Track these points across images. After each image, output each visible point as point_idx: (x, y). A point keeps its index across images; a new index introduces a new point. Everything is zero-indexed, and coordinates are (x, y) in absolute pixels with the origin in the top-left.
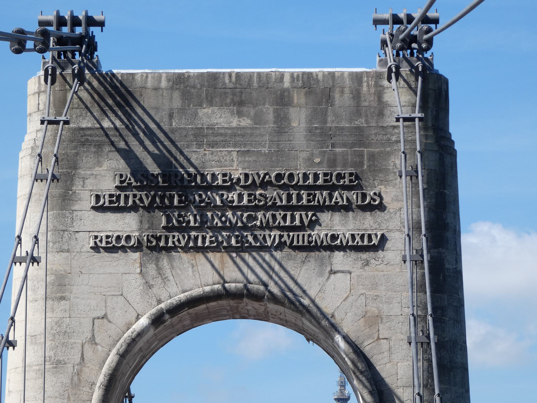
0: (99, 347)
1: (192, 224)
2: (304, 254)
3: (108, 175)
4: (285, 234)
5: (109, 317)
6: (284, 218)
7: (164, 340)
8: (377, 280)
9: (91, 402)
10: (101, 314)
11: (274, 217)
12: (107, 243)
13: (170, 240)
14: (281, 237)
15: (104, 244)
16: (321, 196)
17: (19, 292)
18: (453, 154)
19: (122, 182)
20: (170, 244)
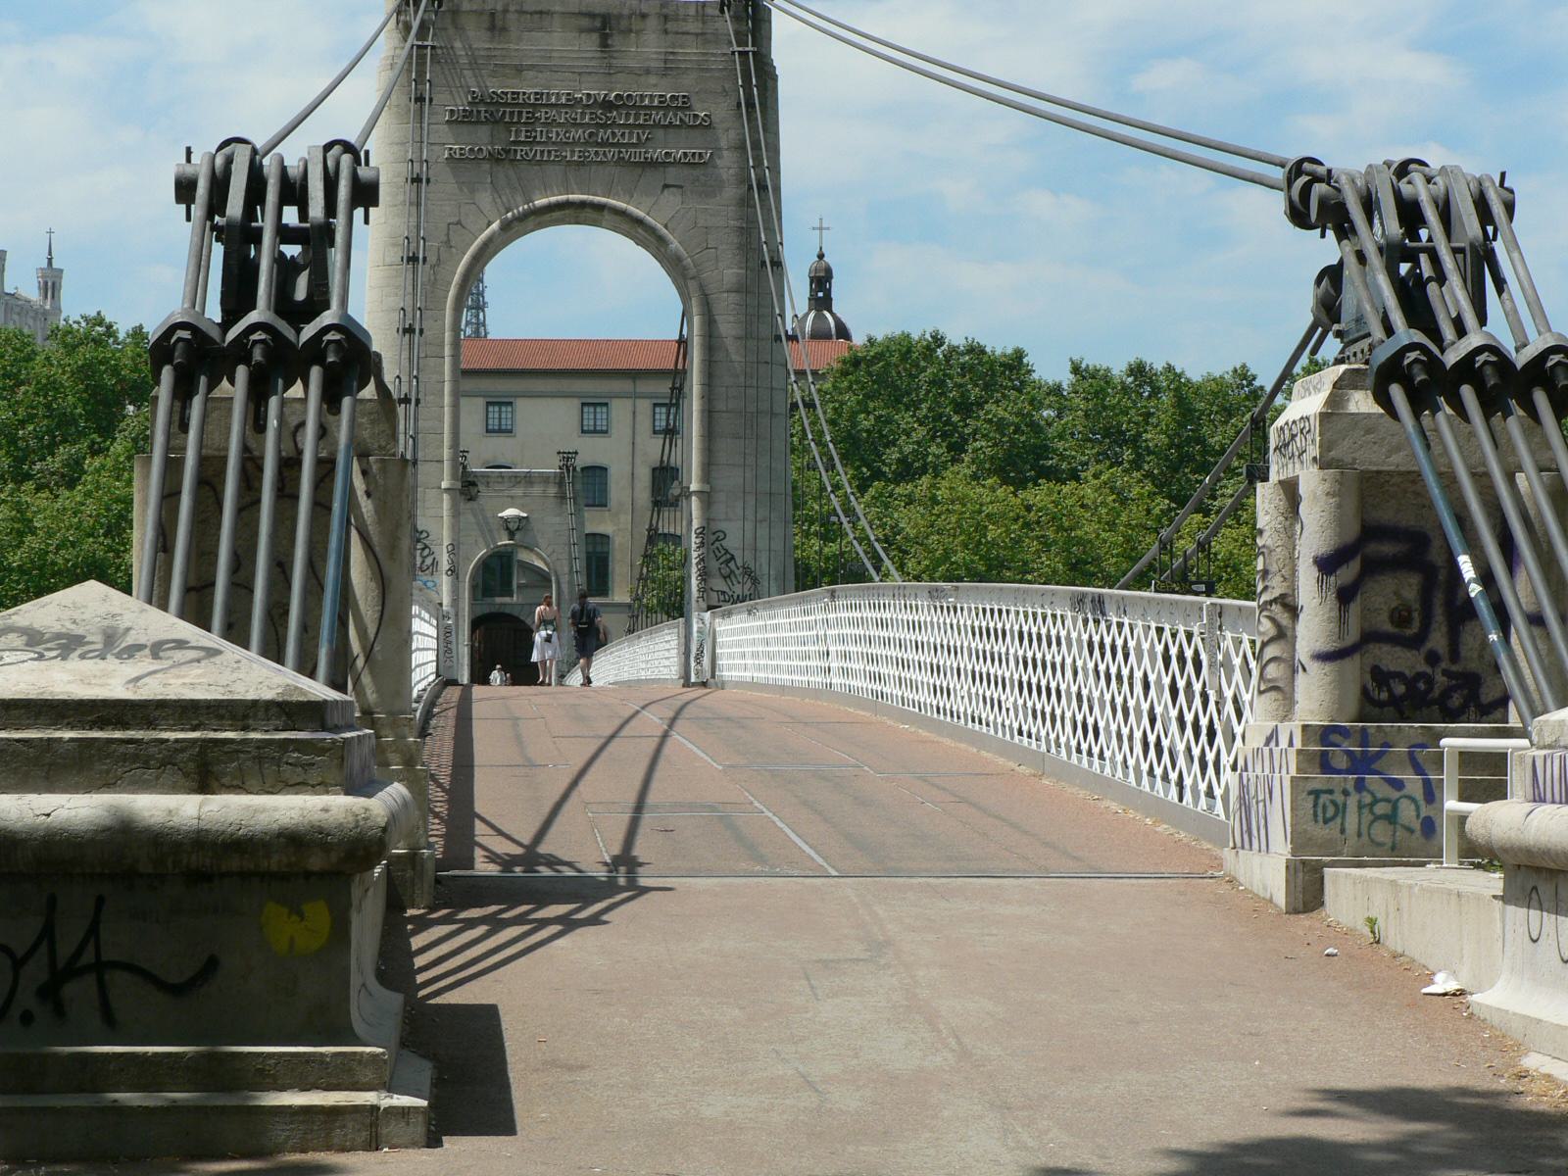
0: (454, 250)
1: (538, 139)
2: (639, 170)
3: (830, 385)
4: (623, 150)
5: (463, 222)
6: (623, 135)
7: (505, 244)
8: (978, 444)
9: (1566, 1028)
10: (454, 219)
11: (613, 133)
12: (461, 154)
13: (519, 153)
14: (620, 152)
15: (458, 156)
16: (657, 116)
17: (284, 129)
18: (775, 78)
19: (473, 98)
20: (518, 157)
